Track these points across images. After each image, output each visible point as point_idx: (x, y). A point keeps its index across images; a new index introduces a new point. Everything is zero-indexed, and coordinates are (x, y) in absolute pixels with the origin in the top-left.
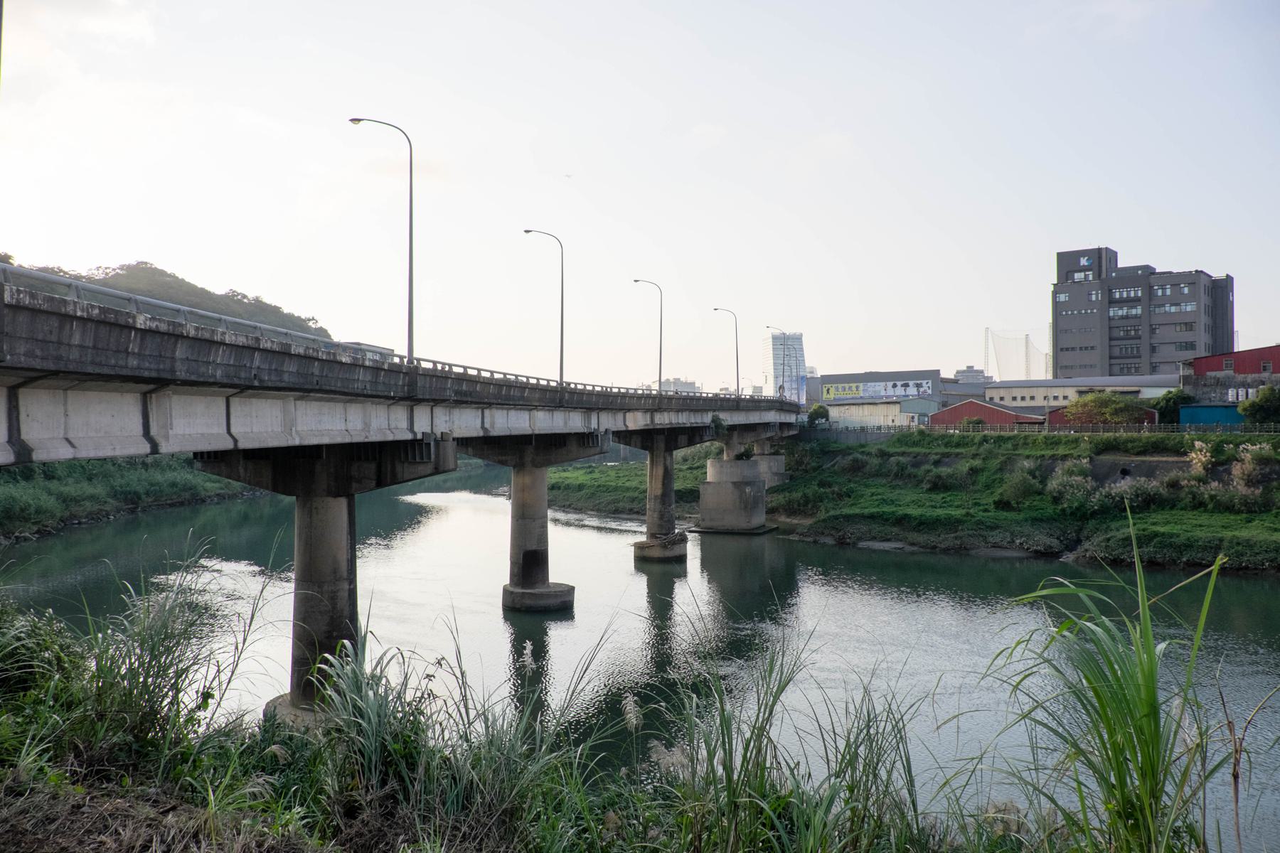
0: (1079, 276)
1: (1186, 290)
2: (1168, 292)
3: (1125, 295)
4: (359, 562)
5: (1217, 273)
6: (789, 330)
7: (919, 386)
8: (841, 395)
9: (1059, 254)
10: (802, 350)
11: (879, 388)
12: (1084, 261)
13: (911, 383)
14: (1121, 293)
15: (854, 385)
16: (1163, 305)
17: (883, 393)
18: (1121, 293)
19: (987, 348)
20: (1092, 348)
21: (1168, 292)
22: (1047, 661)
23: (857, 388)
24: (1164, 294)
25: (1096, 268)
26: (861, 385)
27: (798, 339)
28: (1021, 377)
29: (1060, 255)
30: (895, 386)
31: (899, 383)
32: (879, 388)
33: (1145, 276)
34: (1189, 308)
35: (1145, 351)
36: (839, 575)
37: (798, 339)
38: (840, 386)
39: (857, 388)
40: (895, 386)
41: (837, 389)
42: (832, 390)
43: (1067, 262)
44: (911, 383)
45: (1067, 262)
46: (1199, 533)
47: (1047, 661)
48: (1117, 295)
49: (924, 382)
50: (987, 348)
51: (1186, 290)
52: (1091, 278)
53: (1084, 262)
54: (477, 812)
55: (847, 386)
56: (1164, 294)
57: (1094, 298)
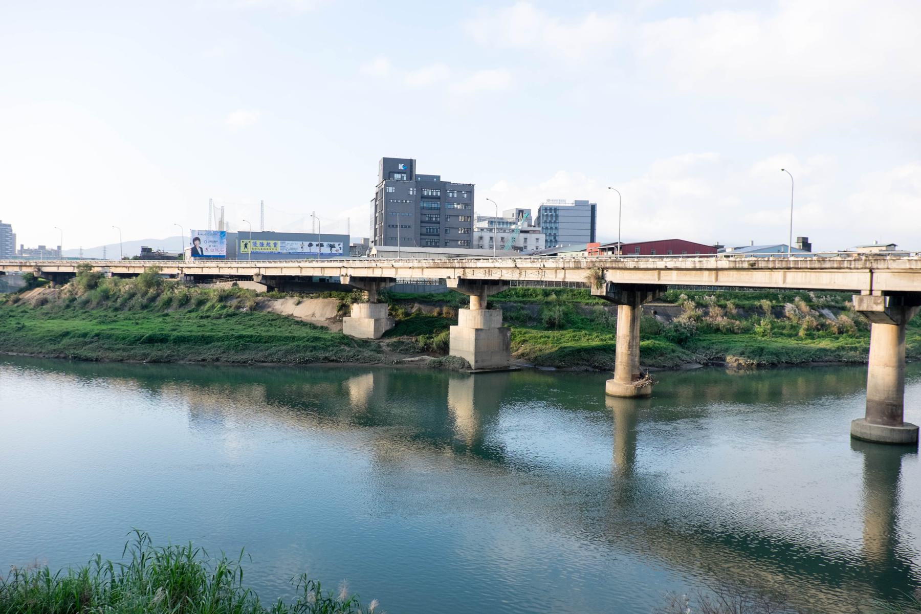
0: (397, 176)
1: (465, 196)
2: (455, 195)
4: (906, 395)
5: (591, 202)
7: (332, 247)
8: (259, 249)
9: (385, 159)
11: (296, 246)
12: (401, 167)
13: (325, 244)
16: (453, 203)
23: (275, 244)
24: (453, 196)
25: (409, 172)
26: (279, 243)
28: (258, 229)
29: (385, 160)
30: (310, 245)
31: (314, 243)
32: (296, 246)
33: (432, 181)
35: (442, 232)
38: (258, 242)
39: (275, 244)
40: (310, 245)
41: (255, 244)
42: (250, 245)
46: (264, 334)
49: (336, 244)
51: (465, 196)
53: (401, 167)
55: (265, 242)
56: (453, 196)
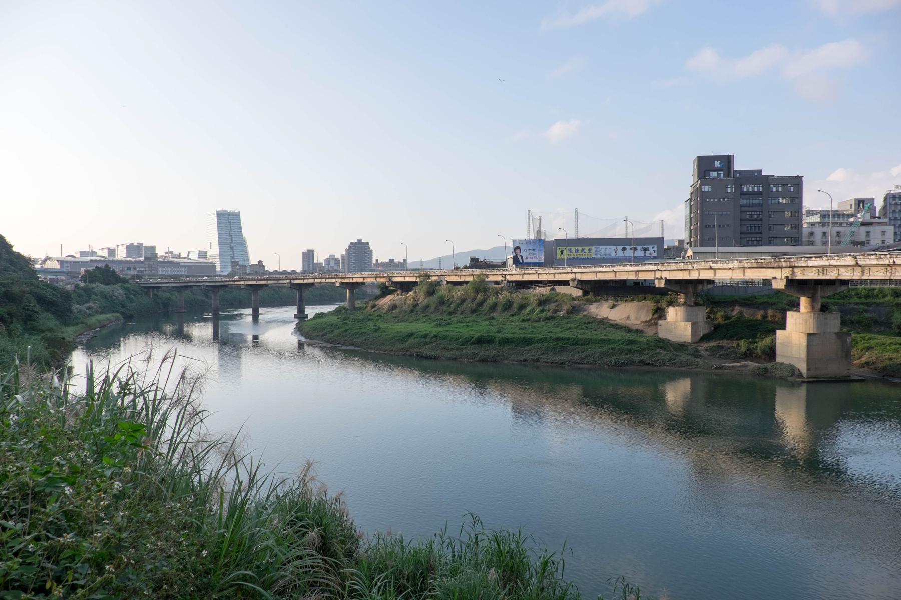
0: (714, 174)
1: (792, 189)
2: (780, 189)
3: (756, 190)
6: (230, 209)
7: (646, 250)
8: (574, 255)
10: (240, 224)
11: (610, 251)
12: (717, 164)
13: (639, 248)
14: (753, 188)
15: (586, 248)
17: (613, 255)
18: (753, 188)
19: (529, 225)
20: (728, 226)
21: (780, 189)
22: (132, 376)
23: (590, 250)
24: (777, 191)
26: (593, 248)
27: (236, 216)
30: (624, 249)
31: (628, 248)
32: (610, 251)
34: (784, 202)
36: (476, 385)
37: (236, 216)
38: (573, 249)
39: (590, 250)
40: (624, 249)
41: (571, 251)
42: (566, 252)
43: (705, 165)
44: (639, 248)
45: (705, 165)
47: (132, 376)
48: (745, 190)
49: (650, 247)
50: (529, 225)
51: (792, 189)
52: (722, 176)
53: (717, 164)
54: (48, 539)
55: (580, 248)
56: (777, 191)
57: (729, 191)
